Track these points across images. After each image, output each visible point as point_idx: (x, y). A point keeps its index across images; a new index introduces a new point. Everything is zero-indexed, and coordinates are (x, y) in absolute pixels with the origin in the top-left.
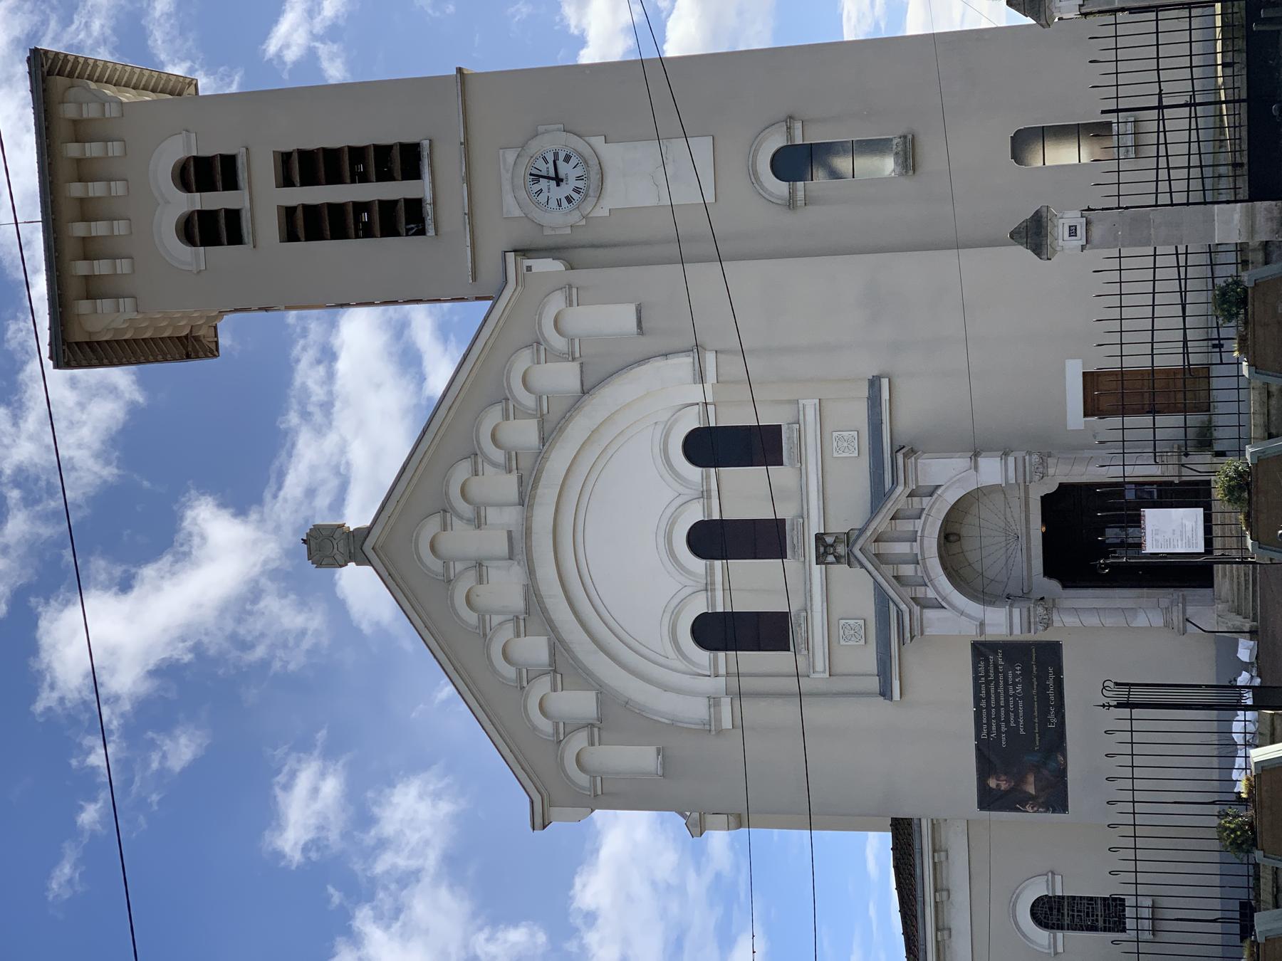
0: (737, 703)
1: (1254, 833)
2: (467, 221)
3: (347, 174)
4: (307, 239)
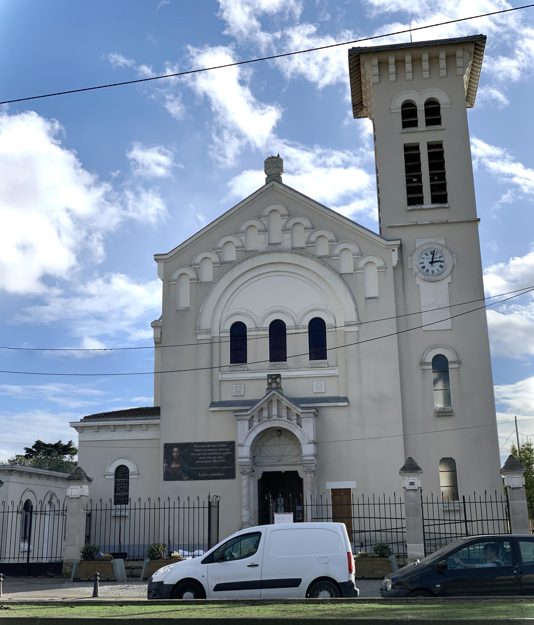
0: (208, 341)
1: (157, 559)
2: (414, 223)
3: (434, 172)
4: (405, 155)
